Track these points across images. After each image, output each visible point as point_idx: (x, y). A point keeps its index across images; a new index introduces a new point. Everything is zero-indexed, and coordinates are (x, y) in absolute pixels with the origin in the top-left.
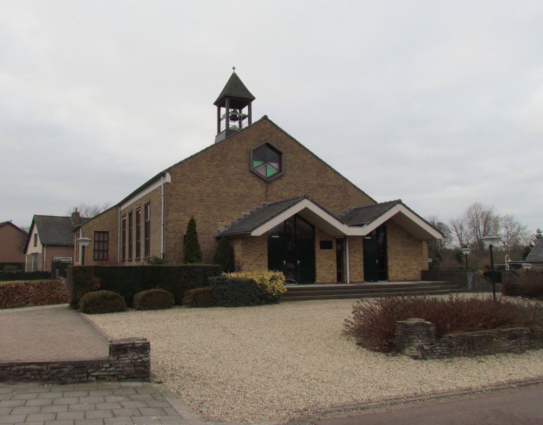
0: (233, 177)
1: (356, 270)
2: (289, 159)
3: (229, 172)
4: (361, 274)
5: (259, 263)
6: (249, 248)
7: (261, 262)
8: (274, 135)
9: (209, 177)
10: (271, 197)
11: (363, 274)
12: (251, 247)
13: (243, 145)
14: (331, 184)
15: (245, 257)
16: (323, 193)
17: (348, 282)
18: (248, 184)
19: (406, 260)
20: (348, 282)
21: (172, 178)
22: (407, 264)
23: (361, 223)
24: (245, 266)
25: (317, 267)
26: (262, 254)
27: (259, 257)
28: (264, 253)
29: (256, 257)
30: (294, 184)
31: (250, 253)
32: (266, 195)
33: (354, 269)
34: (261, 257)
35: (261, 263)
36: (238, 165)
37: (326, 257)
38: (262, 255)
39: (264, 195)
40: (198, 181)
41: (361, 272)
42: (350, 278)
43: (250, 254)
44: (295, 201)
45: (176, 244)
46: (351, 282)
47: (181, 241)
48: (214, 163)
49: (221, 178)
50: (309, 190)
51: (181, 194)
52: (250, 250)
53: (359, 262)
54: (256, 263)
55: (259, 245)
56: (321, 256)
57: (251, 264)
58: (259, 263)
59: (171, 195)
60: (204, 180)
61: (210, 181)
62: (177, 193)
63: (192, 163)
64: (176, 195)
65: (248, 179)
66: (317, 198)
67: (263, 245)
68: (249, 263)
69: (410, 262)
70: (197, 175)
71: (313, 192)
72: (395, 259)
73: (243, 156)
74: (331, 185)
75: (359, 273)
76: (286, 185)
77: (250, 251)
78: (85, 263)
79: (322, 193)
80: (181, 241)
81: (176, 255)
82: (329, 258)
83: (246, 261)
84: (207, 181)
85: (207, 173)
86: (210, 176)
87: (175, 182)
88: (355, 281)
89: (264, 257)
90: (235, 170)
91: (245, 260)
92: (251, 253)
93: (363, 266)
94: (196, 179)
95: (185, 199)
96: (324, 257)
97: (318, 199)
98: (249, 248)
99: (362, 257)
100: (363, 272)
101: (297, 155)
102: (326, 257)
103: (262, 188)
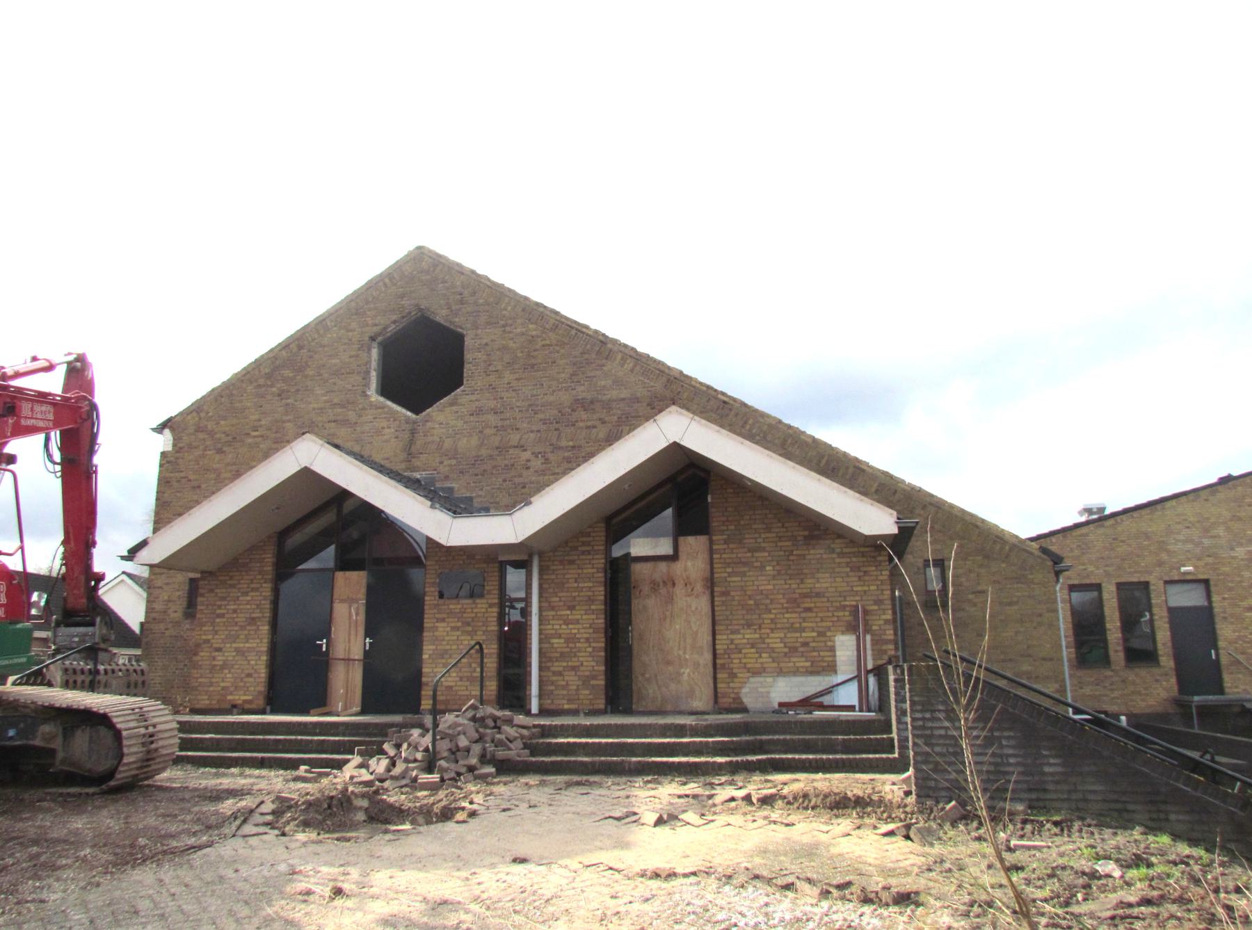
0: (320, 419)
1: (574, 668)
2: (484, 341)
3: (312, 406)
4: (593, 682)
5: (242, 645)
6: (219, 603)
7: (247, 642)
8: (441, 285)
9: (261, 426)
10: (423, 457)
11: (601, 682)
12: (223, 599)
13: (353, 330)
14: (625, 394)
15: (204, 628)
16: (594, 427)
17: (535, 708)
18: (358, 429)
19: (803, 630)
20: (535, 708)
21: (174, 439)
22: (805, 644)
23: (459, 487)
24: (202, 654)
25: (425, 656)
26: (253, 619)
27: (243, 628)
28: (260, 615)
29: (236, 628)
30: (495, 413)
31: (219, 616)
32: (409, 454)
33: (565, 664)
34: (248, 628)
35: (247, 645)
36: (335, 384)
37: (459, 624)
38: (252, 621)
39: (403, 456)
40: (234, 438)
41: (594, 677)
42: (541, 696)
43: (218, 620)
44: (279, 441)
45: (169, 601)
46: (543, 712)
47: (180, 593)
48: (274, 389)
49: (289, 425)
50: (544, 422)
51: (192, 477)
52: (220, 607)
53: (587, 640)
54: (234, 645)
55: (246, 594)
56: (443, 620)
57: (219, 650)
58: (242, 645)
59: (168, 482)
60: (248, 434)
61: (262, 436)
62: (183, 475)
63: (222, 397)
64: (178, 481)
65: (361, 416)
66: (571, 443)
67: (258, 594)
68: (215, 645)
69: (821, 634)
70: (232, 425)
71: (557, 426)
72: (749, 625)
73: (351, 357)
74: (623, 396)
75: (586, 681)
76: (472, 418)
77: (218, 611)
78: (720, 700)
79: (588, 427)
80: (180, 593)
81: (166, 629)
82: (470, 629)
83: (207, 641)
84: (255, 437)
85: (256, 417)
86: (263, 423)
87: (181, 448)
88: (566, 707)
89: (258, 629)
90: (325, 398)
91: (204, 637)
92: (222, 616)
93: (603, 654)
94: (228, 435)
95: (199, 487)
96: (453, 625)
97: (573, 447)
98: (219, 603)
99: (601, 622)
100: (603, 677)
101: (508, 329)
102: (459, 624)
103: (396, 437)
